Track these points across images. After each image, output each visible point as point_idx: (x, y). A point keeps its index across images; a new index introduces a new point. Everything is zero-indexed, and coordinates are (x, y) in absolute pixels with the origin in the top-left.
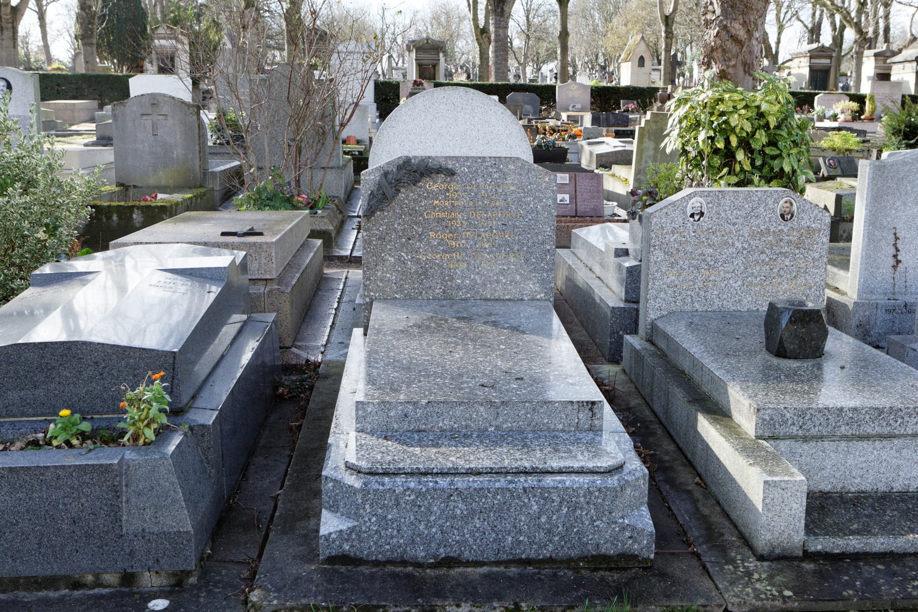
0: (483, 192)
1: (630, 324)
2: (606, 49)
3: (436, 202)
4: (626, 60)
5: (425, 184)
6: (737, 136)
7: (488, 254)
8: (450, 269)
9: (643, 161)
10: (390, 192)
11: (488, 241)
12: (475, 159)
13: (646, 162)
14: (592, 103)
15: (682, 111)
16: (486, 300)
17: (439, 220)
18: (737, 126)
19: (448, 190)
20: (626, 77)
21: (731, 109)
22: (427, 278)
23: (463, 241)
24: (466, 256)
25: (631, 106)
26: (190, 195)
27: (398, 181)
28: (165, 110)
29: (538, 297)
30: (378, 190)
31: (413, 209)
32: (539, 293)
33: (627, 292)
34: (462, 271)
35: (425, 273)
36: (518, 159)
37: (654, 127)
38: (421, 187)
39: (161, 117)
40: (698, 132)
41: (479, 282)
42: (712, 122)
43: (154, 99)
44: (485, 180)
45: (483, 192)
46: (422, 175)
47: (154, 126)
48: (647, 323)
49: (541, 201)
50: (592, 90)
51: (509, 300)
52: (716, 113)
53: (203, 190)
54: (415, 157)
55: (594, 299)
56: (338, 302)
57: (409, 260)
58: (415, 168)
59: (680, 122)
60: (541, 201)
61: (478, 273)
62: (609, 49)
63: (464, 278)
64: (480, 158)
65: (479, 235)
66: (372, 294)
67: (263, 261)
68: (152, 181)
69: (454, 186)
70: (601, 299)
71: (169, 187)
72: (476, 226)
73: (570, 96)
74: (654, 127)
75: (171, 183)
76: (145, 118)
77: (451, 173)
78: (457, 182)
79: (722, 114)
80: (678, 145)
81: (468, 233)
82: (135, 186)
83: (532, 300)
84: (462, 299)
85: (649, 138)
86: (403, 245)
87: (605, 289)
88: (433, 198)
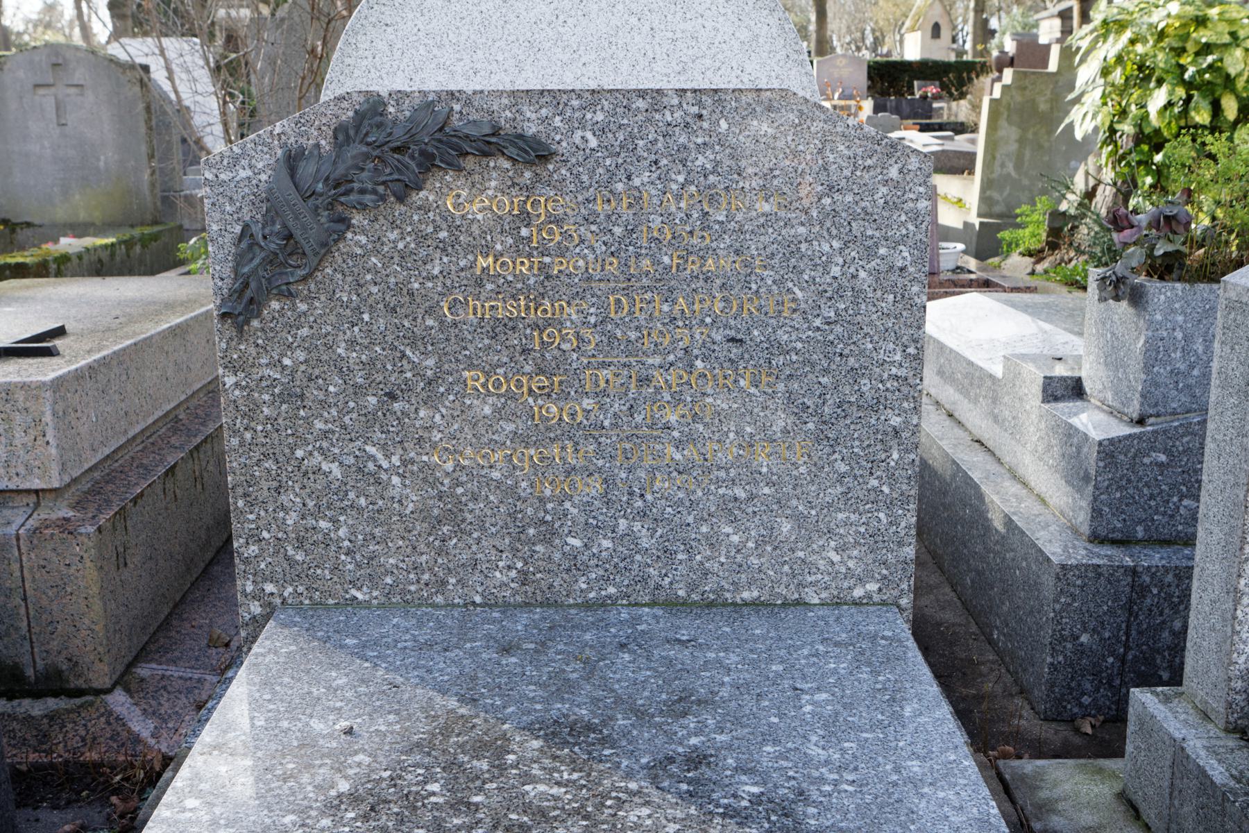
0: (657, 221)
1: (1111, 611)
2: (877, 22)
3: (482, 262)
4: (912, 29)
5: (440, 194)
6: (1238, 98)
7: (678, 445)
8: (542, 500)
9: (997, 163)
10: (310, 229)
11: (677, 400)
12: (624, 98)
13: (1003, 165)
14: (869, 88)
15: (1111, 48)
16: (674, 605)
17: (498, 329)
18: (1239, 75)
19: (525, 218)
20: (913, 49)
21: (1227, 39)
22: (460, 532)
23: (588, 403)
24: (599, 453)
25: (932, 90)
26: (114, 240)
27: (340, 184)
28: (79, 76)
29: (858, 592)
30: (269, 219)
31: (399, 288)
32: (861, 581)
33: (1096, 513)
34: (587, 507)
35: (454, 516)
36: (784, 93)
37: (1019, 99)
38: (424, 208)
39: (72, 91)
40: (1147, 93)
41: (645, 543)
42: (1183, 69)
43: (57, 54)
44: (665, 179)
45: (657, 221)
46: (428, 163)
47: (59, 107)
48: (1235, 671)
49: (870, 253)
50: (869, 67)
51: (755, 604)
52: (1191, 47)
53: (156, 229)
54: (400, 96)
55: (987, 527)
56: (192, 584)
57: (393, 470)
58: (399, 135)
59: (1105, 72)
60: (870, 253)
61: (643, 514)
62: (881, 23)
63: (592, 530)
64: (642, 94)
65: (645, 381)
66: (270, 588)
67: (19, 437)
68: (61, 213)
69: (546, 203)
70: (1009, 522)
71: (93, 224)
72: (631, 348)
73: (836, 75)
74: (1019, 99)
75: (97, 216)
76: (41, 91)
77: (537, 153)
78: (559, 186)
79: (1206, 49)
80: (1103, 119)
81: (604, 373)
82: (29, 225)
83: (837, 603)
84: (587, 606)
85: (1009, 120)
86: (370, 418)
87: (1013, 488)
88: (470, 249)
